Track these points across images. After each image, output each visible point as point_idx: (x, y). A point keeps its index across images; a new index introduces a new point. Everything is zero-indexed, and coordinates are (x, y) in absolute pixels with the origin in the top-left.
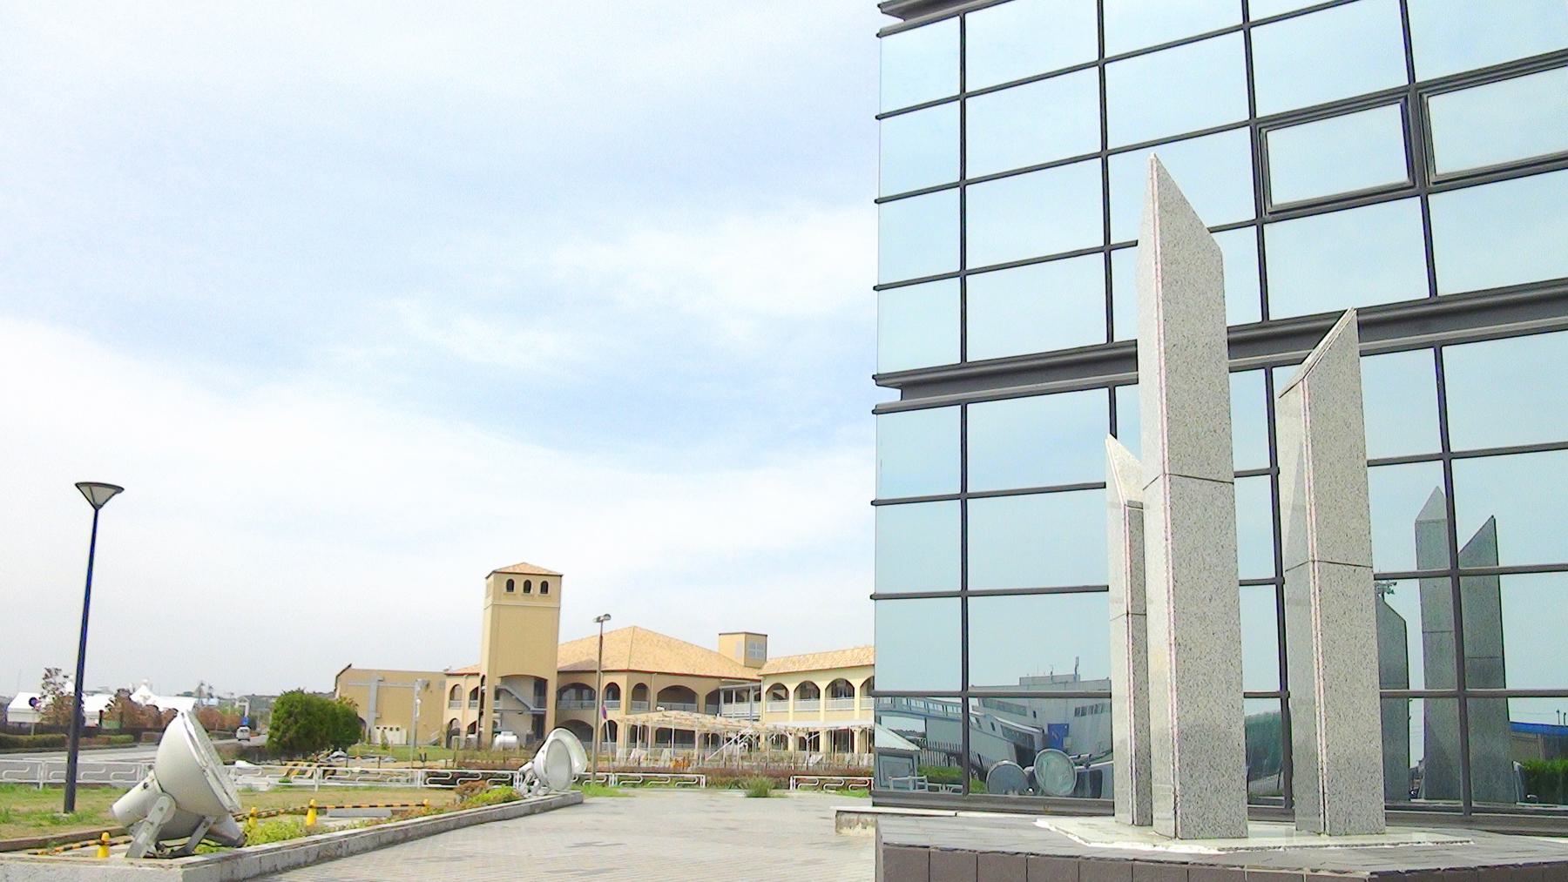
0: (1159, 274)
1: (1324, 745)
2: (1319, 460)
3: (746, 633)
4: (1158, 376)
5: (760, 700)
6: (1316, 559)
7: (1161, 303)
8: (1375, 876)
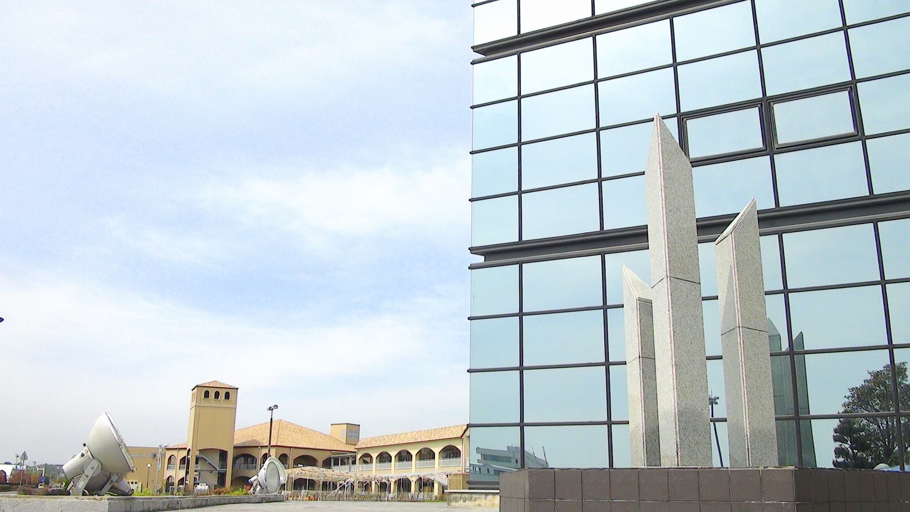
0: (662, 174)
1: (748, 423)
2: (740, 275)
3: (347, 424)
4: (663, 226)
5: (355, 464)
6: (741, 326)
7: (663, 189)
8: (797, 469)
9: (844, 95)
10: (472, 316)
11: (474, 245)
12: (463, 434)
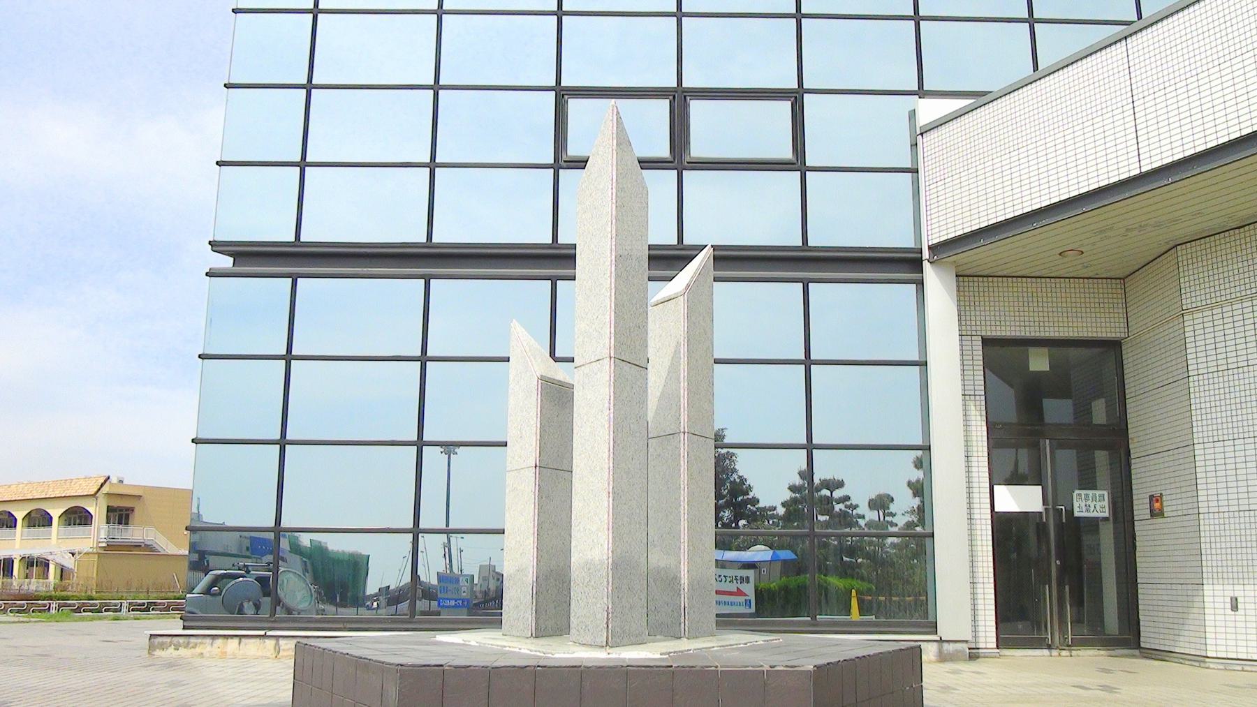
0: (614, 197)
1: (686, 571)
4: (609, 279)
6: (686, 431)
7: (614, 221)
9: (785, 107)
10: (206, 353)
11: (218, 238)
12: (99, 490)
